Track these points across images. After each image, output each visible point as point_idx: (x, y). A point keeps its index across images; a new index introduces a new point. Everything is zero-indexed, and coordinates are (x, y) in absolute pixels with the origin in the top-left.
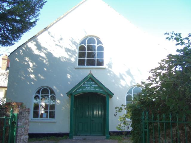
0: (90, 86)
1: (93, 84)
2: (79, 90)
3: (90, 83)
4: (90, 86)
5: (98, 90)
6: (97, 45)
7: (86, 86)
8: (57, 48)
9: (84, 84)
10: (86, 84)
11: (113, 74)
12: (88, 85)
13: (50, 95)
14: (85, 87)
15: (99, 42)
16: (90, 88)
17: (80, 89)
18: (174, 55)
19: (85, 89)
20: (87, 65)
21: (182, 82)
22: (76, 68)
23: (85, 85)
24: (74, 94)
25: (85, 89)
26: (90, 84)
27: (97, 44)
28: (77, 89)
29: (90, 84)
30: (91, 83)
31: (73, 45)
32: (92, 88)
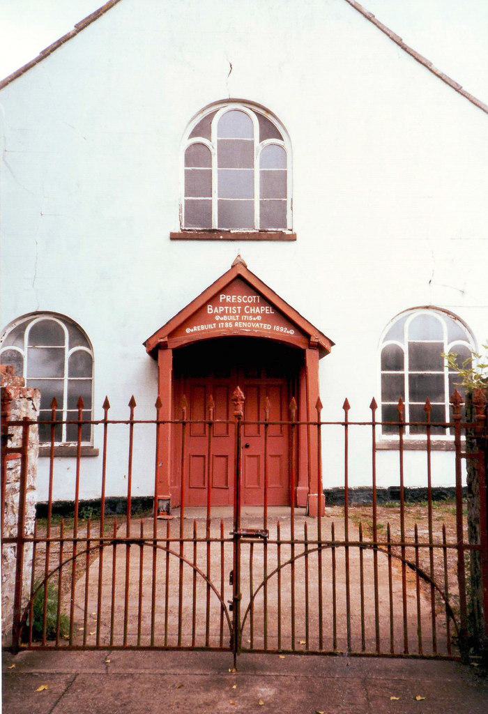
1: (252, 305)
3: (240, 299)
4: (243, 313)
26: (243, 305)
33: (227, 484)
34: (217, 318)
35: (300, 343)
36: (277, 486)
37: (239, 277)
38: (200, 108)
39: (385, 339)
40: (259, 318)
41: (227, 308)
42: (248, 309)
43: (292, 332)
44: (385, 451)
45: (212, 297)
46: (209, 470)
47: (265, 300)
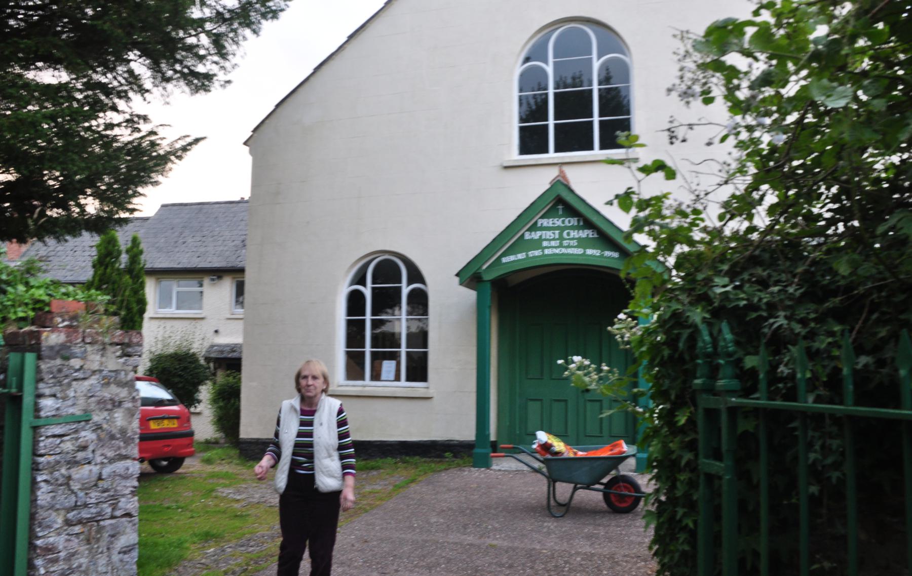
0: (561, 238)
1: (573, 228)
2: (512, 258)
3: (558, 222)
4: (561, 238)
5: (596, 252)
6: (599, 57)
7: (541, 240)
8: (669, 90)
9: (534, 227)
10: (543, 228)
11: (785, 228)
12: (549, 234)
13: (599, 57)
14: (537, 244)
15: (415, 275)
16: (561, 246)
17: (515, 254)
18: (249, 159)
19: (537, 253)
20: (558, 149)
21: (861, 123)
22: (506, 168)
23: (536, 235)
24: (488, 277)
25: (537, 253)
26: (561, 229)
27: (409, 283)
28: (505, 254)
29: (558, 228)
30: (563, 222)
31: (764, 203)
32: (569, 247)
33: (601, 432)
34: (545, 244)
35: (624, 270)
36: (184, 441)
37: (560, 201)
38: (524, 41)
39: (527, 60)
40: (575, 243)
41: (544, 232)
42: (568, 234)
43: (616, 255)
44: (501, 458)
45: (525, 217)
46: (585, 411)
47: (588, 224)
